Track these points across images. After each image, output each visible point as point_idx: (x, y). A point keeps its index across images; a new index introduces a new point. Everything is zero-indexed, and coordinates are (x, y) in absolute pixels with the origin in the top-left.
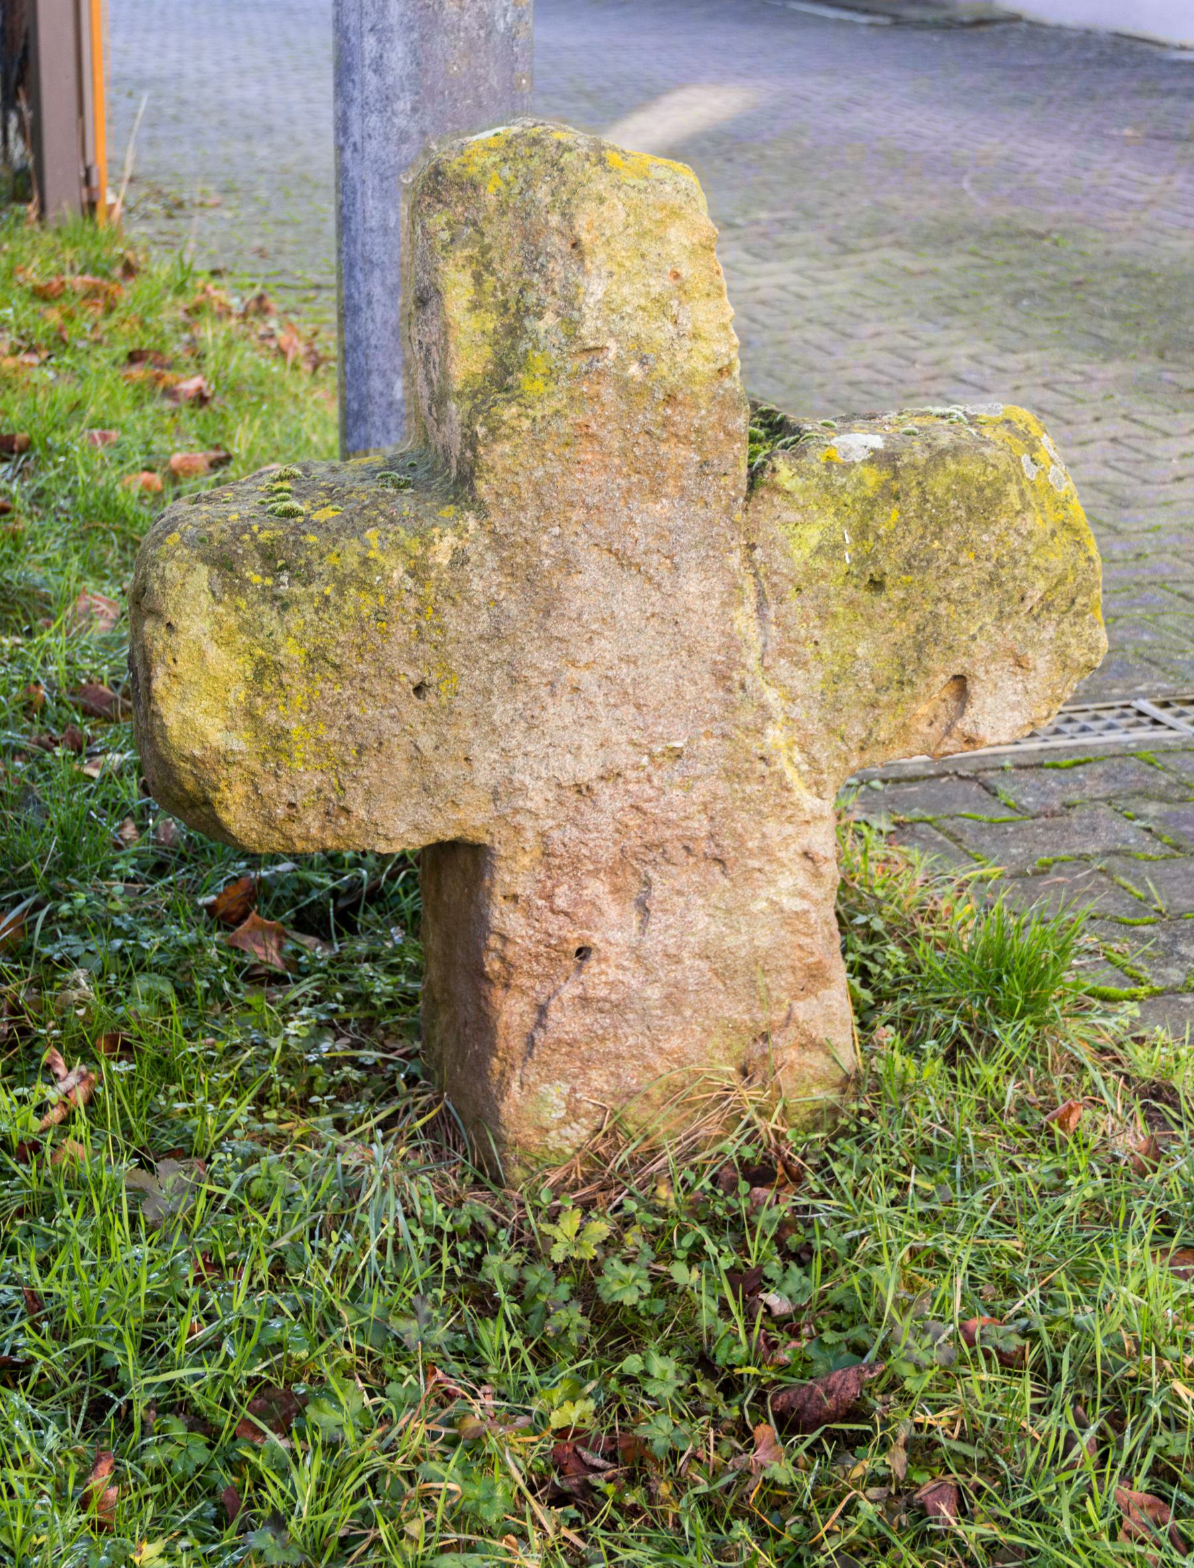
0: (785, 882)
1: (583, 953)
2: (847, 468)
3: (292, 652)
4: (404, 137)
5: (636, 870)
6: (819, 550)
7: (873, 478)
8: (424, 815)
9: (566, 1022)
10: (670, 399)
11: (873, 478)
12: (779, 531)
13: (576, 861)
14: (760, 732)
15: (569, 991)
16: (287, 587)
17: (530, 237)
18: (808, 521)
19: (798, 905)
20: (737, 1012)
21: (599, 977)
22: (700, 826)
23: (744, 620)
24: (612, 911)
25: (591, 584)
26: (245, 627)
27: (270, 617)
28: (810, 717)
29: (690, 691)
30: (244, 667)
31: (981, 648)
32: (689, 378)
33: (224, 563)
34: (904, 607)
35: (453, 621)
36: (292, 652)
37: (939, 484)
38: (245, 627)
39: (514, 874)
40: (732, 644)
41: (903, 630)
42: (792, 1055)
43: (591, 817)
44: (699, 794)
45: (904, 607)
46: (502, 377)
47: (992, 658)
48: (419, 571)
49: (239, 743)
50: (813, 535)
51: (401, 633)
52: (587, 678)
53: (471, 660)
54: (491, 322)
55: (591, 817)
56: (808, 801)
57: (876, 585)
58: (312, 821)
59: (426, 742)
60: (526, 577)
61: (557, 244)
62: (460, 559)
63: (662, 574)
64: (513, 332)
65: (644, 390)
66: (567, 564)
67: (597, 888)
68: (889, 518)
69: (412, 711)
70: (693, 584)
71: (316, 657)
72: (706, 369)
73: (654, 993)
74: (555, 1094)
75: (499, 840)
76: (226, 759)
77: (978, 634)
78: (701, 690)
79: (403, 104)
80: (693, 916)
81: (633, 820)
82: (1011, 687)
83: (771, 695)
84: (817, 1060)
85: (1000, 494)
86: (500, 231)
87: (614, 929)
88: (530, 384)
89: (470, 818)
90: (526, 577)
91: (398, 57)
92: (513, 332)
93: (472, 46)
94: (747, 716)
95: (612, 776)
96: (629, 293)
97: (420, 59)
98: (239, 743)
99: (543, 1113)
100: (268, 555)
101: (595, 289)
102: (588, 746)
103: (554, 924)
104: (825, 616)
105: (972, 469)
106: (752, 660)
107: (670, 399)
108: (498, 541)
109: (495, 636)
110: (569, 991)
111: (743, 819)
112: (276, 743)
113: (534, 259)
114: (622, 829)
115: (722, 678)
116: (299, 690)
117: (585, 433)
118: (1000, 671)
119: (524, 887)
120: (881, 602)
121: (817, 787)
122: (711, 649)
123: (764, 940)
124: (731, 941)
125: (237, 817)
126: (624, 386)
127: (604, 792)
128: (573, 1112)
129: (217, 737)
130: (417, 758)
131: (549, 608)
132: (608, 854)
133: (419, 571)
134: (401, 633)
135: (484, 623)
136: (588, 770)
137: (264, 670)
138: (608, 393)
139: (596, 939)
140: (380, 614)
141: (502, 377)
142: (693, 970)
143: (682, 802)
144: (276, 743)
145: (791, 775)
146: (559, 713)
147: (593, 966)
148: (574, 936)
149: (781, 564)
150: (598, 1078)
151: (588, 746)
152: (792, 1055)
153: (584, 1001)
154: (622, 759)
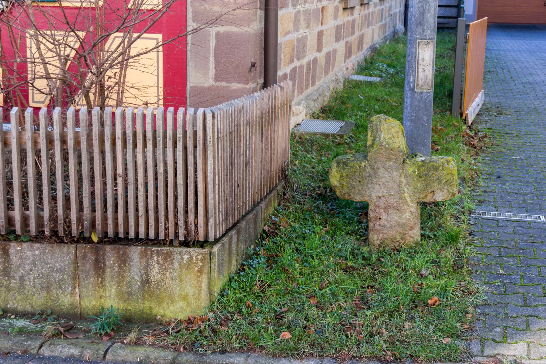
0: (407, 214)
1: (380, 218)
2: (417, 162)
3: (344, 175)
4: (409, 113)
5: (386, 208)
6: (413, 171)
7: (420, 163)
8: (360, 197)
9: (377, 227)
10: (392, 150)
11: (420, 163)
12: (407, 168)
13: (379, 206)
14: (404, 194)
15: (378, 223)
16: (345, 167)
17: (377, 128)
18: (411, 167)
19: (409, 218)
20: (400, 230)
21: (382, 222)
22: (395, 204)
23: (402, 179)
24: (384, 214)
25: (381, 171)
26: (339, 171)
27: (342, 170)
28: (411, 193)
29: (395, 187)
30: (339, 176)
31: (436, 188)
32: (394, 148)
33: (338, 163)
34: (425, 181)
35: (364, 174)
36: (344, 175)
37: (430, 165)
38: (339, 171)
39: (371, 207)
40: (400, 182)
41: (425, 184)
42: (408, 238)
43: (381, 201)
44: (395, 200)
45: (425, 181)
46: (372, 145)
47: (437, 189)
48: (360, 167)
49: (338, 185)
50: (412, 169)
51: (358, 174)
52: (381, 183)
53: (366, 179)
54: (372, 138)
55: (381, 201)
56: (411, 204)
57: (421, 177)
58: (347, 196)
59: (360, 188)
60: (373, 169)
61: (379, 130)
62: (365, 166)
63: (391, 172)
64: (374, 140)
65: (388, 148)
66: (378, 168)
67: (382, 210)
68: (422, 169)
69: (359, 184)
70: (395, 174)
71: (347, 176)
72: (396, 147)
73: (389, 225)
74: (375, 237)
75: (369, 202)
76: (336, 186)
77: (435, 186)
78: (396, 187)
79: (409, 108)
80: (394, 216)
81: (386, 202)
82: (441, 194)
83: (406, 189)
84: (411, 239)
85: (439, 168)
86: (375, 127)
87: (384, 216)
88: (375, 146)
89: (366, 199)
90: (373, 169)
91: (409, 101)
92: (374, 140)
93: (419, 100)
94: (402, 191)
95: (383, 196)
96: (387, 137)
97: (411, 102)
98: (338, 185)
99: (375, 238)
100: (344, 163)
101: (382, 136)
102: (381, 192)
103: (376, 214)
104: (413, 180)
105: (435, 164)
106: (403, 184)
107: (392, 150)
108: (370, 165)
109: (369, 176)
110: (378, 223)
111: (401, 205)
112: (342, 185)
113: (377, 131)
114: (385, 203)
115: (399, 186)
116: (345, 179)
117: (380, 153)
118: (439, 191)
119: (372, 209)
120: (421, 180)
121: (412, 202)
122: (398, 182)
123: (404, 221)
124: (399, 221)
125: (338, 193)
126: (386, 148)
127: (383, 198)
128: (378, 239)
129: (336, 184)
130: (359, 190)
131: (376, 173)
132: (383, 206)
133: (360, 167)
134: (358, 174)
135: (368, 174)
136: (380, 195)
137: (341, 176)
138: (384, 148)
139: (381, 217)
140: (355, 172)
141: (372, 145)
142: (394, 223)
143: (393, 201)
144: (342, 185)
145: (408, 200)
146: (377, 187)
147: (381, 220)
148: (379, 216)
149: (407, 172)
150: (381, 235)
151: (381, 192)
152: (408, 238)
153: (380, 225)
154: (385, 194)
